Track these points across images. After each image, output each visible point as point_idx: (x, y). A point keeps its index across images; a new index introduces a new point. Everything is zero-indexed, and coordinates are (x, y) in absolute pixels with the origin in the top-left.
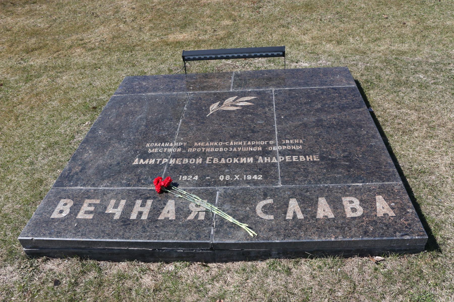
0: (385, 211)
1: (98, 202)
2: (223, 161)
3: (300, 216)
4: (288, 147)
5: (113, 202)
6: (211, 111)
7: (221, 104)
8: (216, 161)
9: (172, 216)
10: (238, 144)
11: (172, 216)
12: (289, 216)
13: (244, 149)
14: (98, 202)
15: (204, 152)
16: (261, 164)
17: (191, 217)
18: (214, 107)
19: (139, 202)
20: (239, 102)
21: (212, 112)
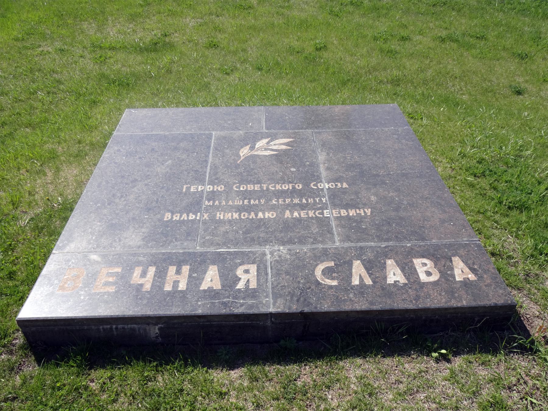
0: (398, 278)
1: (119, 270)
2: (260, 215)
3: (368, 281)
4: (239, 202)
5: (138, 271)
6: (242, 155)
7: (252, 148)
8: (168, 218)
9: (217, 285)
10: (232, 216)
11: (217, 285)
12: (356, 281)
13: (237, 203)
14: (119, 270)
15: (189, 213)
16: (261, 219)
17: (241, 285)
18: (244, 152)
19: (172, 270)
20: (274, 145)
21: (244, 157)
